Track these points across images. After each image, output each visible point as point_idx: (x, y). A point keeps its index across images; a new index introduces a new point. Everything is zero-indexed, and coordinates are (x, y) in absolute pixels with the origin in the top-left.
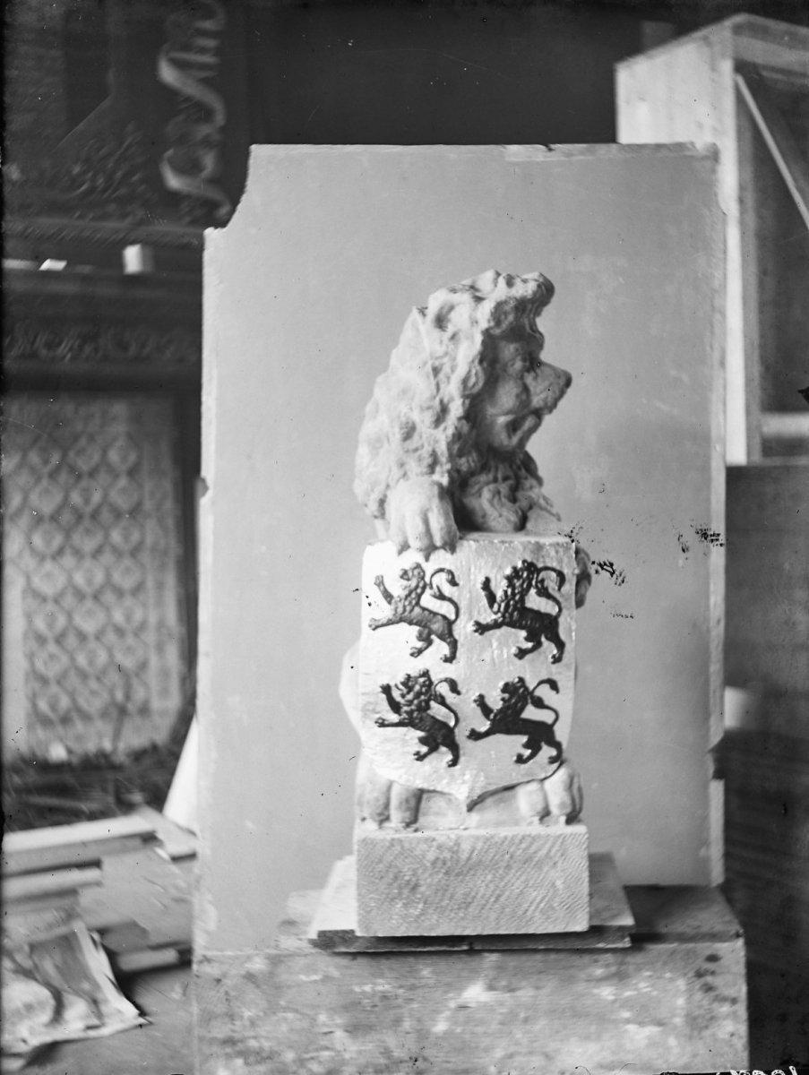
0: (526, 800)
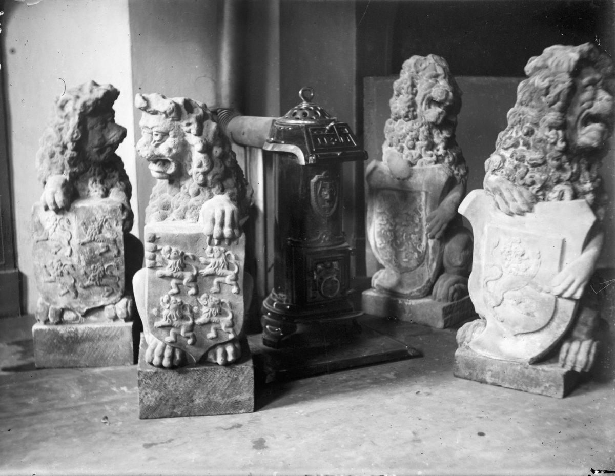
0: (107, 313)
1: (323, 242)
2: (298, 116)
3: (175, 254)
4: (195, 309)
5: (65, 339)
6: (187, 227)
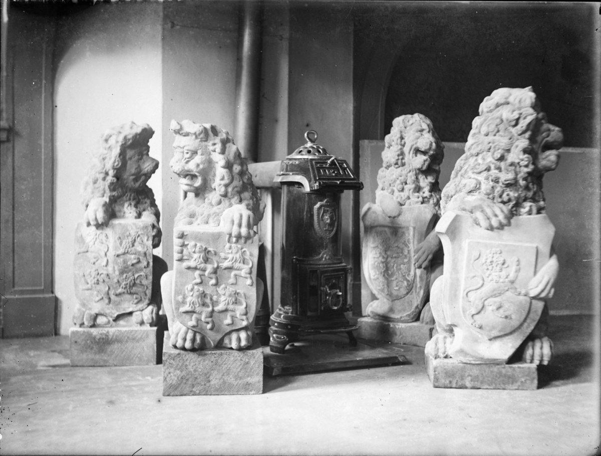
0: (135, 318)
1: (324, 259)
2: (303, 153)
3: (200, 248)
4: (215, 298)
5: (97, 340)
6: (211, 228)
